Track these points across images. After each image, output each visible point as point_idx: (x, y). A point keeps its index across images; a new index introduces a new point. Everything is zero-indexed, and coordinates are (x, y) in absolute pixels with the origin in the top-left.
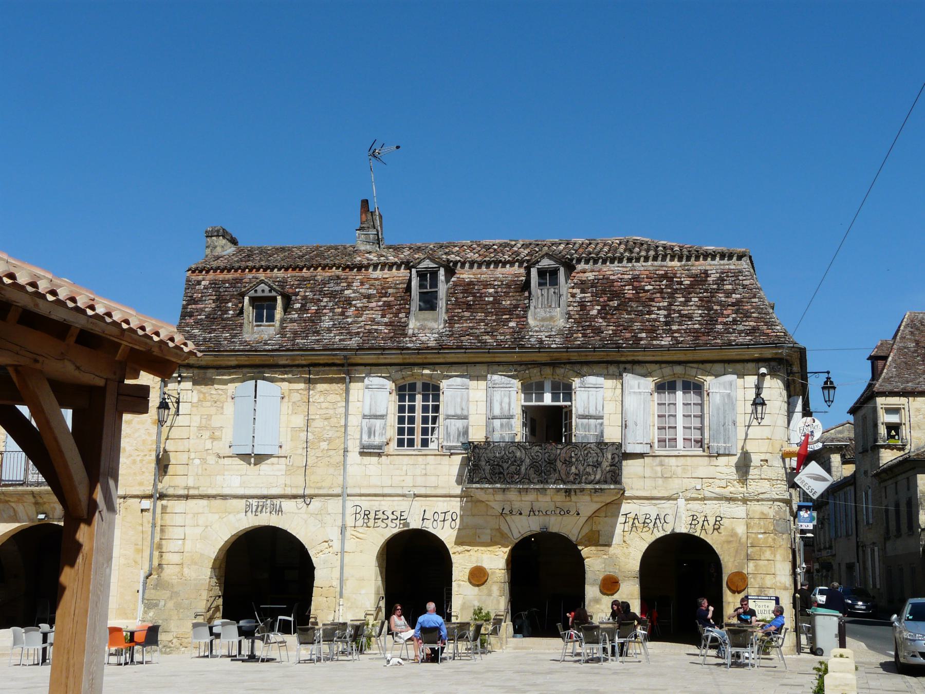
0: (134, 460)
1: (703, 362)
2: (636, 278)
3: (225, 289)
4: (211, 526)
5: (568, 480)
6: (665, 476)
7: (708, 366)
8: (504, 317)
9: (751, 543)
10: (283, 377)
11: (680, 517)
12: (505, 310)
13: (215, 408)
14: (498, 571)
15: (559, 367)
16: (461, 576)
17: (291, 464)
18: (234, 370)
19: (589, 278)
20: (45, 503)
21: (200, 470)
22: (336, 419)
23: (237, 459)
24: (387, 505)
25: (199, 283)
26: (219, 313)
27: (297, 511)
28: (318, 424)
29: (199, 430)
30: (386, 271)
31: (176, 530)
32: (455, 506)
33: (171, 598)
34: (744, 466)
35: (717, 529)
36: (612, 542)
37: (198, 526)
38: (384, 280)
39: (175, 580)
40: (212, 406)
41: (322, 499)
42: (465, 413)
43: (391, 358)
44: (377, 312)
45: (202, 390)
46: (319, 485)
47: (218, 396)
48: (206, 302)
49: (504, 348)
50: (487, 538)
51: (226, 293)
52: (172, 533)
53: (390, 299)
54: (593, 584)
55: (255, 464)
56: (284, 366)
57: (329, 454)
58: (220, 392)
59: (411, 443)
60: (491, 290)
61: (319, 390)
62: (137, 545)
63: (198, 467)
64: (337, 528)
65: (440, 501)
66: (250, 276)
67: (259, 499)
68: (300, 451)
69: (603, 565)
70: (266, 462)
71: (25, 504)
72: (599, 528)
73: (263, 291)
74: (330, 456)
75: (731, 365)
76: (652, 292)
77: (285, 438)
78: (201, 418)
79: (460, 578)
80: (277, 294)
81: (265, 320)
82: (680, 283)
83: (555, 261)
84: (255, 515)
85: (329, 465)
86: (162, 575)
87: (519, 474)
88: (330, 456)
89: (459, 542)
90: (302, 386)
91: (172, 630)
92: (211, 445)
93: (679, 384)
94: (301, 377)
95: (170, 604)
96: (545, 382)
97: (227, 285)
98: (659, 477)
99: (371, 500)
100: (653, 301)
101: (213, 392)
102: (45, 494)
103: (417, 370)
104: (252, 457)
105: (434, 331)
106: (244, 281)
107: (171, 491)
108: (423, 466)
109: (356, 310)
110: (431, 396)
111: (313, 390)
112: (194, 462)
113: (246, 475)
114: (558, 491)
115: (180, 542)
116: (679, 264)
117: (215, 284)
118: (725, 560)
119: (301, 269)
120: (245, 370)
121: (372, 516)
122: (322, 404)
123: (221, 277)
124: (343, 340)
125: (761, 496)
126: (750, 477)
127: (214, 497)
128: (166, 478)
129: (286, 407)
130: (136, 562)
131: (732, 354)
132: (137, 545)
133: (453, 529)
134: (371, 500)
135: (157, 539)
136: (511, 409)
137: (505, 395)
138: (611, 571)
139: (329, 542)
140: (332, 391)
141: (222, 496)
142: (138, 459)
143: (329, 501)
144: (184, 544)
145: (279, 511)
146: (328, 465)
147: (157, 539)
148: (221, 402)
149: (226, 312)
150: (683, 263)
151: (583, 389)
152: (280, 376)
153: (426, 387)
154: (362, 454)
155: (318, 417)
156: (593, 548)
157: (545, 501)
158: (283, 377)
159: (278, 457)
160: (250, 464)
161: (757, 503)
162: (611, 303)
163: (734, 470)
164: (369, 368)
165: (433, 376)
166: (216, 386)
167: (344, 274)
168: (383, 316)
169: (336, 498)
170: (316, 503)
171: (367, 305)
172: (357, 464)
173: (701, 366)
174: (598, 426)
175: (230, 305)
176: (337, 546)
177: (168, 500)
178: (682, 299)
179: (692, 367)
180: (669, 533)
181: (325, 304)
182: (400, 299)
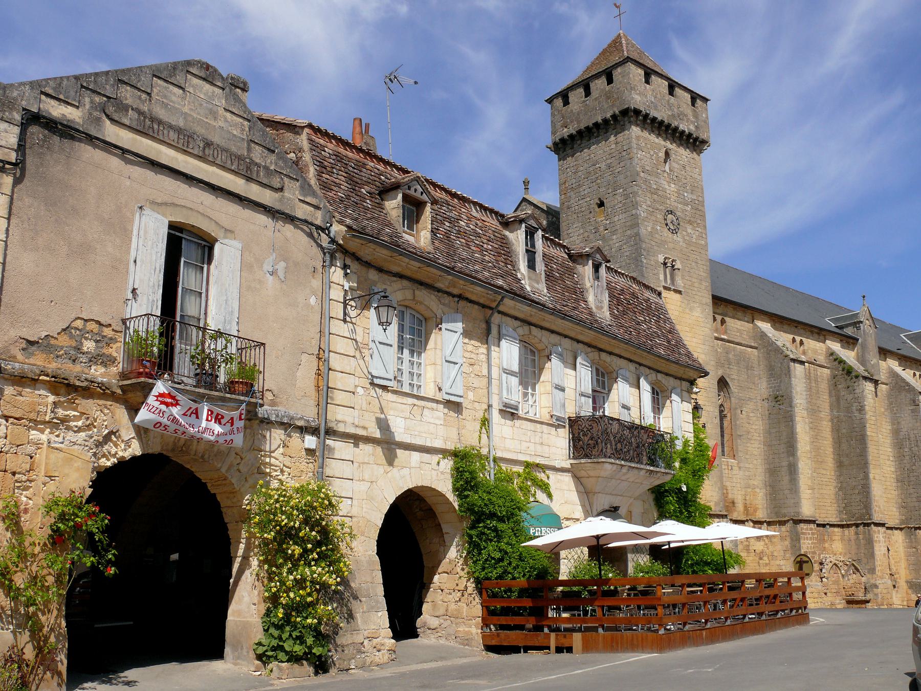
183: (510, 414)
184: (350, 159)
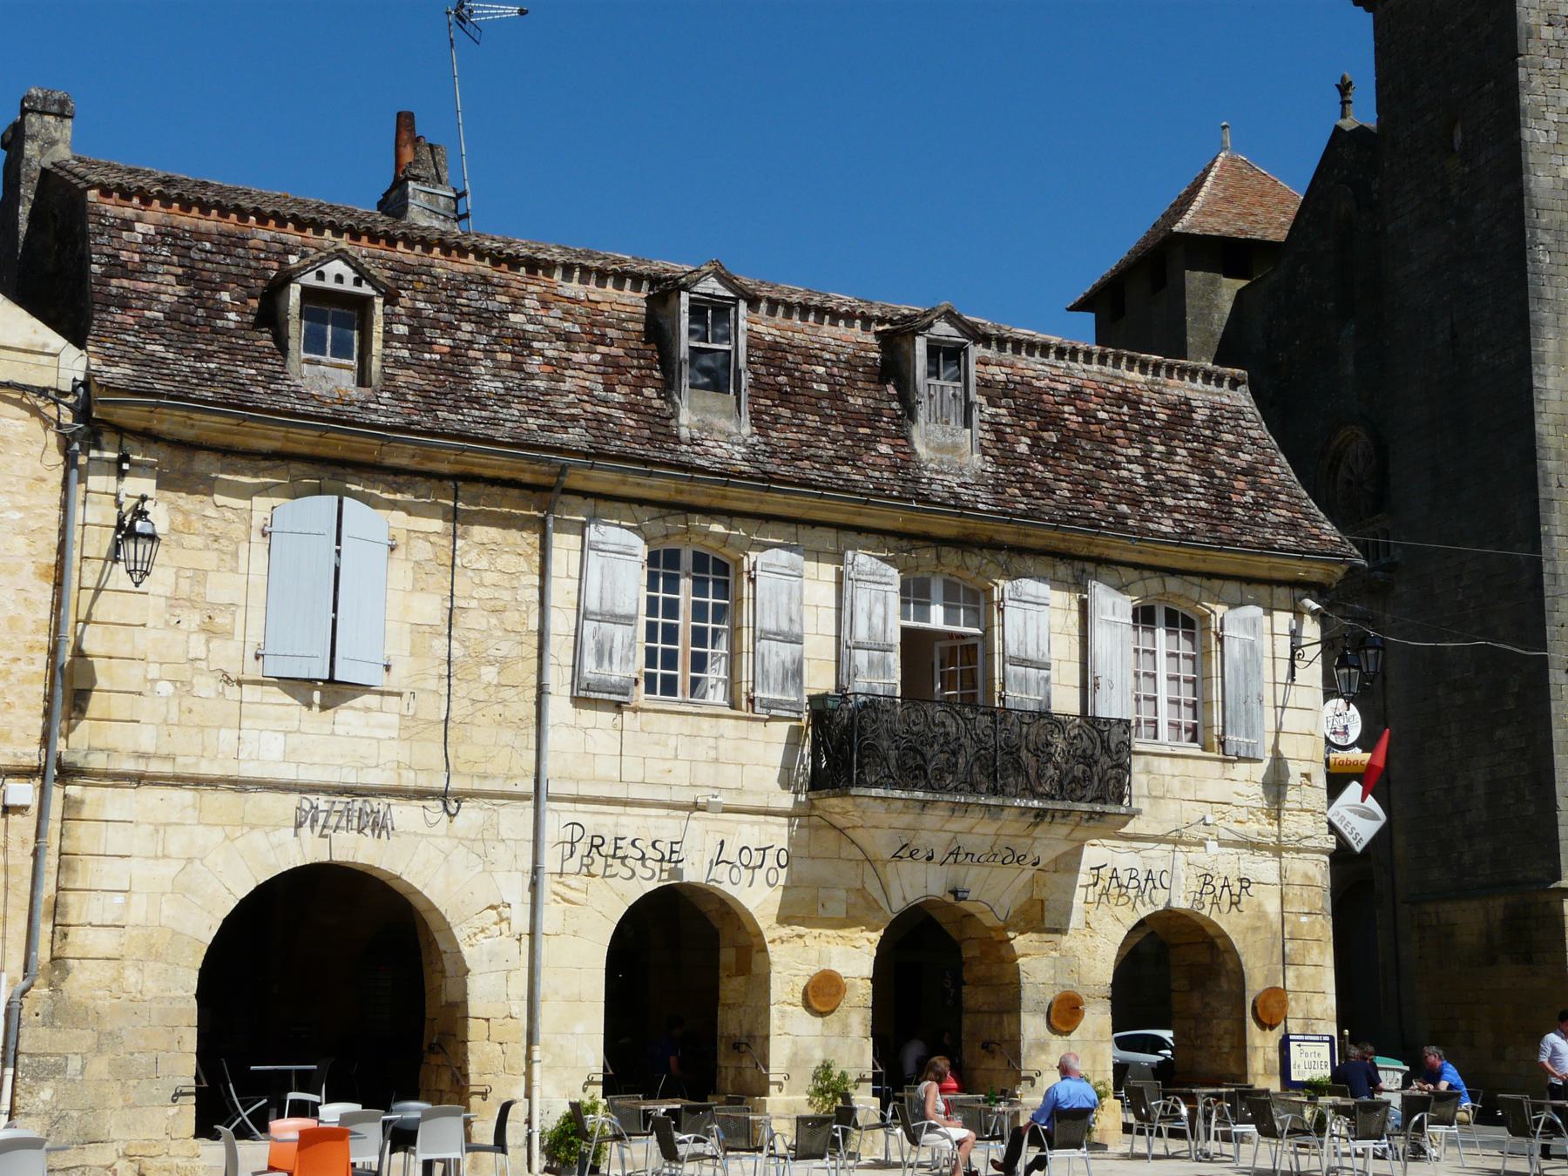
1: (1210, 576)
2: (1076, 394)
3: (203, 255)
4: (201, 860)
5: (1040, 790)
6: (1154, 794)
7: (1217, 583)
8: (862, 430)
9: (1291, 933)
10: (391, 497)
11: (1179, 878)
12: (860, 416)
13: (215, 553)
14: (859, 982)
15: (971, 552)
16: (787, 994)
17: (411, 712)
19: (998, 378)
22: (516, 614)
23: (275, 689)
24: (631, 824)
25: (128, 225)
27: (427, 831)
28: (473, 621)
30: (592, 286)
31: (107, 865)
32: (777, 834)
33: (99, 1049)
34: (1276, 784)
35: (1236, 904)
36: (1068, 924)
37: (165, 856)
38: (593, 305)
39: (104, 1002)
40: (207, 548)
41: (485, 803)
42: (796, 629)
43: (651, 487)
44: (592, 376)
45: (181, 502)
46: (481, 769)
47: (223, 524)
49: (891, 497)
50: (839, 911)
52: (89, 873)
53: (615, 351)
54: (1035, 1012)
55: (323, 707)
56: (397, 471)
57: (501, 695)
58: (229, 515)
59: (670, 686)
60: (821, 370)
61: (477, 539)
64: (520, 874)
65: (745, 822)
67: (329, 795)
68: (432, 684)
69: (1052, 972)
70: (351, 703)
72: (1045, 894)
73: (339, 278)
74: (503, 702)
75: (1253, 587)
76: (1108, 424)
77: (398, 648)
78: (177, 577)
79: (785, 997)
80: (374, 293)
81: (329, 350)
82: (1152, 416)
83: (960, 330)
85: (502, 721)
87: (953, 773)
88: (503, 702)
89: (784, 919)
90: (437, 525)
91: (114, 1135)
92: (204, 648)
93: (1160, 616)
94: (435, 503)
95: (99, 1066)
96: (933, 582)
98: (1143, 796)
99: (598, 813)
100: (1116, 444)
101: (211, 512)
103: (697, 521)
104: (317, 688)
105: (734, 439)
106: (251, 243)
107: (98, 762)
108: (711, 742)
109: (546, 364)
110: (711, 583)
111: (463, 538)
112: (158, 688)
113: (299, 731)
114: (1023, 814)
116: (1142, 378)
117: (175, 237)
118: (1250, 965)
119: (392, 242)
120: (296, 468)
121: (607, 849)
122: (484, 574)
124: (550, 429)
125: (1306, 843)
126: (1287, 805)
127: (213, 783)
128: (84, 726)
129: (401, 571)
131: (1262, 566)
133: (771, 886)
134: (598, 813)
135: (48, 889)
136: (888, 631)
137: (877, 599)
138: (1069, 983)
139: (500, 909)
140: (508, 545)
141: (235, 782)
143: (502, 810)
144: (127, 904)
146: (500, 724)
148: (230, 539)
149: (219, 311)
150: (1149, 377)
151: (1016, 604)
152: (385, 496)
153: (700, 561)
154: (579, 701)
155: (474, 604)
156: (1034, 936)
157: (977, 830)
158: (391, 497)
159: (382, 693)
160: (309, 705)
161: (1295, 855)
162: (1045, 435)
163: (1259, 790)
164: (591, 501)
165: (730, 540)
166: (220, 499)
167: (497, 274)
168: (609, 388)
169: (519, 803)
170: (471, 814)
171: (566, 355)
172: (568, 726)
173: (1205, 583)
174: (1042, 683)
176: (520, 918)
177: (85, 785)
178: (1161, 448)
179: (1193, 584)
180: (1160, 908)
181: (467, 337)
182: (635, 354)
183: (612, 706)
184: (199, 235)
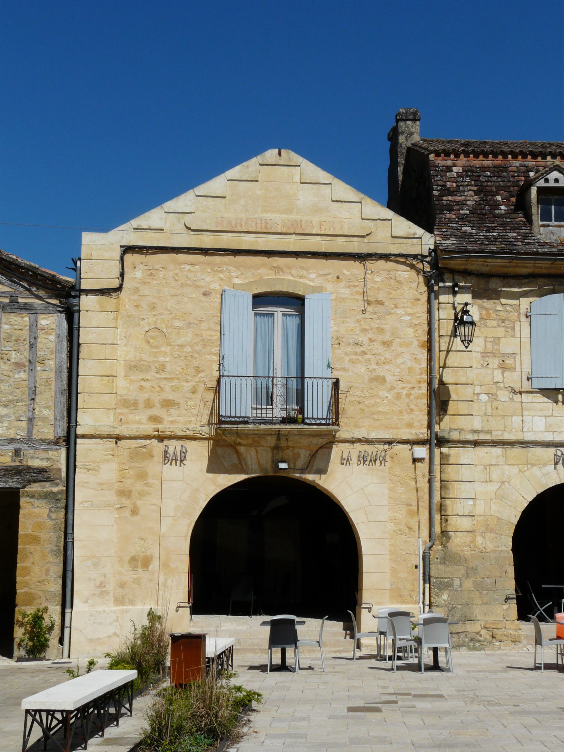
0: (399, 393)
4: (508, 482)
13: (503, 329)
18: (526, 280)
20: (288, 448)
21: (489, 408)
23: (539, 395)
26: (487, 208)
29: (484, 356)
33: (467, 576)
37: (491, 481)
40: (499, 326)
45: (485, 304)
47: (506, 313)
48: (466, 193)
51: (489, 183)
52: (457, 490)
58: (508, 308)
62: (411, 505)
63: (485, 405)
66: (517, 164)
71: (259, 449)
78: (486, 342)
81: (553, 218)
84: (385, 466)
86: (448, 545)
91: (479, 617)
92: (501, 376)
95: (468, 584)
97: (488, 173)
101: (499, 308)
102: (295, 435)
104: (560, 393)
106: (510, 169)
107: (455, 436)
113: (552, 415)
115: (470, 502)
117: (472, 171)
120: (541, 281)
123: (477, 163)
130: (410, 528)
132: (411, 505)
135: (437, 498)
142: (405, 392)
145: (172, 460)
147: (437, 498)
149: (496, 205)
160: (557, 402)
166: (503, 301)
175: (499, 198)
177: (450, 447)
